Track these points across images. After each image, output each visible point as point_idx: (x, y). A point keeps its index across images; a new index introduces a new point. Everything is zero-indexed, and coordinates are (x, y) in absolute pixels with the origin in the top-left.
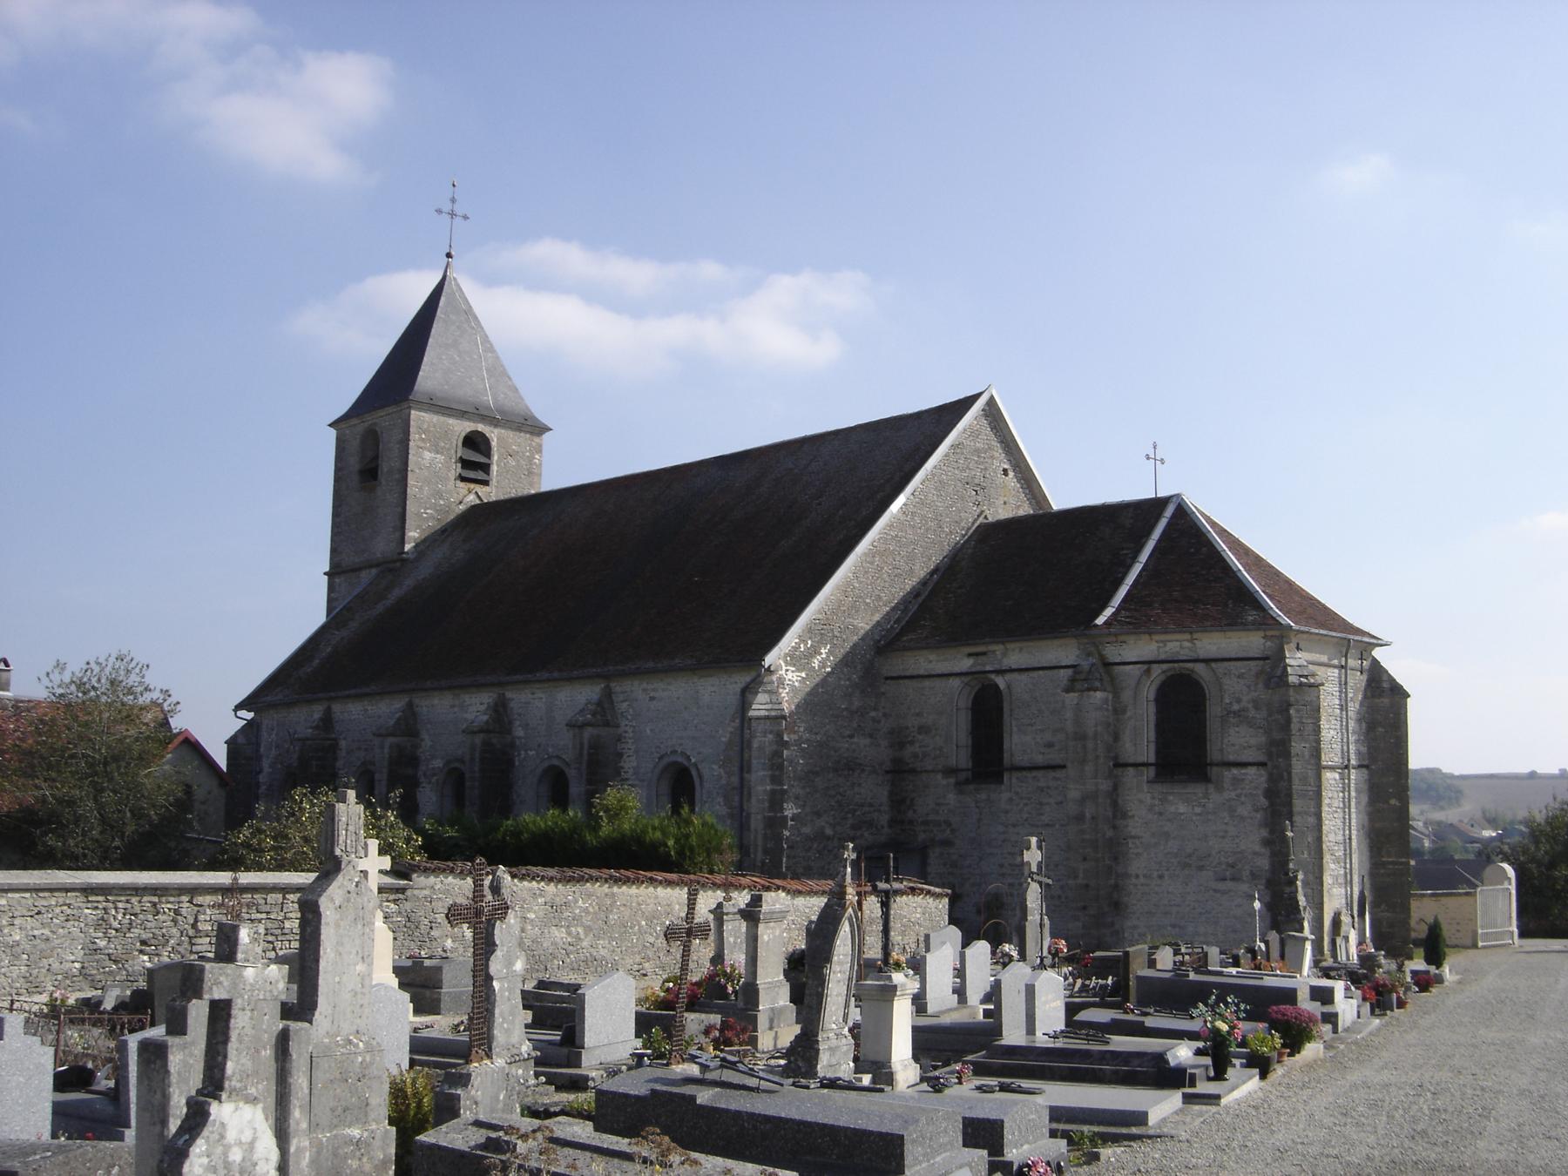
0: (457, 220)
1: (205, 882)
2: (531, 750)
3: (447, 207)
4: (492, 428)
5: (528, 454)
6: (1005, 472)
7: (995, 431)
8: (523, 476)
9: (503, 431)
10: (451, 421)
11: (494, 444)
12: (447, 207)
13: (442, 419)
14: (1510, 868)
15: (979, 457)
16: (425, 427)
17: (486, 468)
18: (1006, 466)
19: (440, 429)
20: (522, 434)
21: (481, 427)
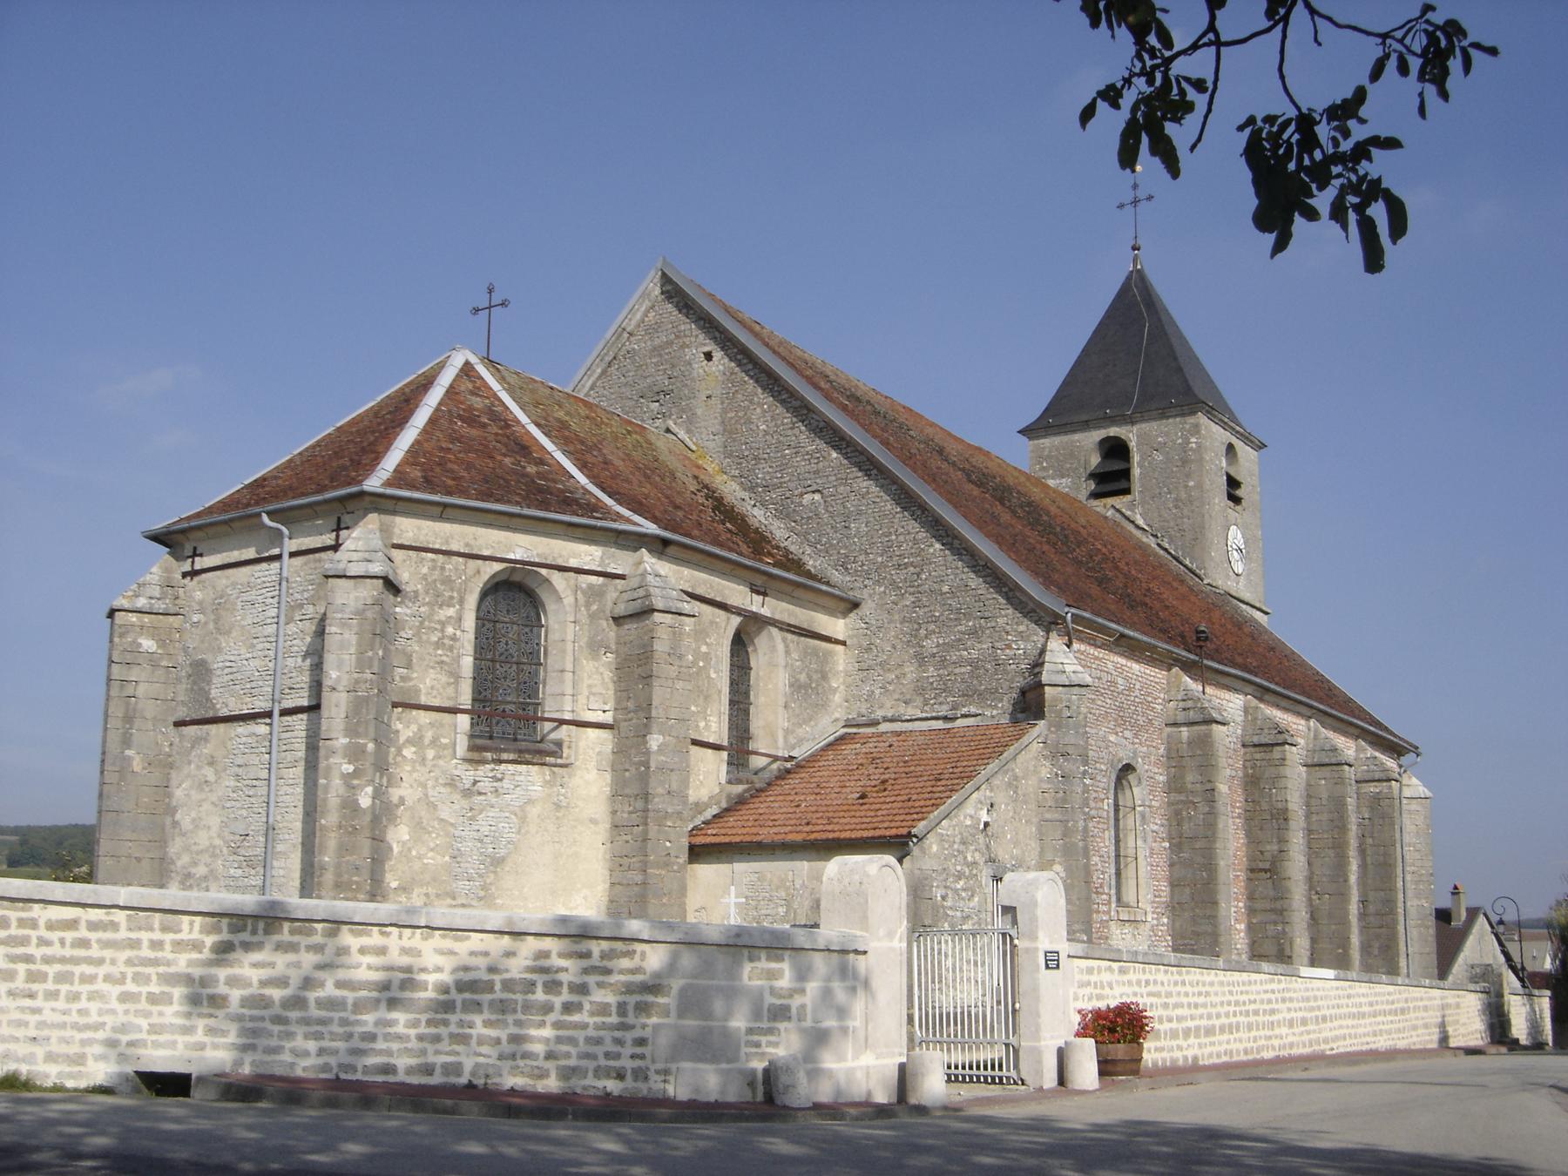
0: (1143, 205)
1: (1474, 931)
2: (445, 737)
3: (1141, 194)
4: (1129, 427)
5: (1180, 441)
6: (708, 356)
7: (684, 311)
8: (1174, 469)
9: (1143, 425)
10: (1076, 437)
11: (1133, 445)
12: (1129, 197)
13: (1065, 438)
14: (380, 1080)
15: (660, 355)
16: (1046, 453)
17: (1126, 474)
18: (707, 349)
19: (1064, 449)
20: (1171, 420)
21: (1113, 431)
